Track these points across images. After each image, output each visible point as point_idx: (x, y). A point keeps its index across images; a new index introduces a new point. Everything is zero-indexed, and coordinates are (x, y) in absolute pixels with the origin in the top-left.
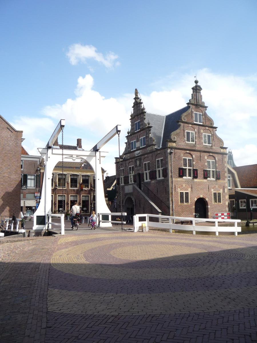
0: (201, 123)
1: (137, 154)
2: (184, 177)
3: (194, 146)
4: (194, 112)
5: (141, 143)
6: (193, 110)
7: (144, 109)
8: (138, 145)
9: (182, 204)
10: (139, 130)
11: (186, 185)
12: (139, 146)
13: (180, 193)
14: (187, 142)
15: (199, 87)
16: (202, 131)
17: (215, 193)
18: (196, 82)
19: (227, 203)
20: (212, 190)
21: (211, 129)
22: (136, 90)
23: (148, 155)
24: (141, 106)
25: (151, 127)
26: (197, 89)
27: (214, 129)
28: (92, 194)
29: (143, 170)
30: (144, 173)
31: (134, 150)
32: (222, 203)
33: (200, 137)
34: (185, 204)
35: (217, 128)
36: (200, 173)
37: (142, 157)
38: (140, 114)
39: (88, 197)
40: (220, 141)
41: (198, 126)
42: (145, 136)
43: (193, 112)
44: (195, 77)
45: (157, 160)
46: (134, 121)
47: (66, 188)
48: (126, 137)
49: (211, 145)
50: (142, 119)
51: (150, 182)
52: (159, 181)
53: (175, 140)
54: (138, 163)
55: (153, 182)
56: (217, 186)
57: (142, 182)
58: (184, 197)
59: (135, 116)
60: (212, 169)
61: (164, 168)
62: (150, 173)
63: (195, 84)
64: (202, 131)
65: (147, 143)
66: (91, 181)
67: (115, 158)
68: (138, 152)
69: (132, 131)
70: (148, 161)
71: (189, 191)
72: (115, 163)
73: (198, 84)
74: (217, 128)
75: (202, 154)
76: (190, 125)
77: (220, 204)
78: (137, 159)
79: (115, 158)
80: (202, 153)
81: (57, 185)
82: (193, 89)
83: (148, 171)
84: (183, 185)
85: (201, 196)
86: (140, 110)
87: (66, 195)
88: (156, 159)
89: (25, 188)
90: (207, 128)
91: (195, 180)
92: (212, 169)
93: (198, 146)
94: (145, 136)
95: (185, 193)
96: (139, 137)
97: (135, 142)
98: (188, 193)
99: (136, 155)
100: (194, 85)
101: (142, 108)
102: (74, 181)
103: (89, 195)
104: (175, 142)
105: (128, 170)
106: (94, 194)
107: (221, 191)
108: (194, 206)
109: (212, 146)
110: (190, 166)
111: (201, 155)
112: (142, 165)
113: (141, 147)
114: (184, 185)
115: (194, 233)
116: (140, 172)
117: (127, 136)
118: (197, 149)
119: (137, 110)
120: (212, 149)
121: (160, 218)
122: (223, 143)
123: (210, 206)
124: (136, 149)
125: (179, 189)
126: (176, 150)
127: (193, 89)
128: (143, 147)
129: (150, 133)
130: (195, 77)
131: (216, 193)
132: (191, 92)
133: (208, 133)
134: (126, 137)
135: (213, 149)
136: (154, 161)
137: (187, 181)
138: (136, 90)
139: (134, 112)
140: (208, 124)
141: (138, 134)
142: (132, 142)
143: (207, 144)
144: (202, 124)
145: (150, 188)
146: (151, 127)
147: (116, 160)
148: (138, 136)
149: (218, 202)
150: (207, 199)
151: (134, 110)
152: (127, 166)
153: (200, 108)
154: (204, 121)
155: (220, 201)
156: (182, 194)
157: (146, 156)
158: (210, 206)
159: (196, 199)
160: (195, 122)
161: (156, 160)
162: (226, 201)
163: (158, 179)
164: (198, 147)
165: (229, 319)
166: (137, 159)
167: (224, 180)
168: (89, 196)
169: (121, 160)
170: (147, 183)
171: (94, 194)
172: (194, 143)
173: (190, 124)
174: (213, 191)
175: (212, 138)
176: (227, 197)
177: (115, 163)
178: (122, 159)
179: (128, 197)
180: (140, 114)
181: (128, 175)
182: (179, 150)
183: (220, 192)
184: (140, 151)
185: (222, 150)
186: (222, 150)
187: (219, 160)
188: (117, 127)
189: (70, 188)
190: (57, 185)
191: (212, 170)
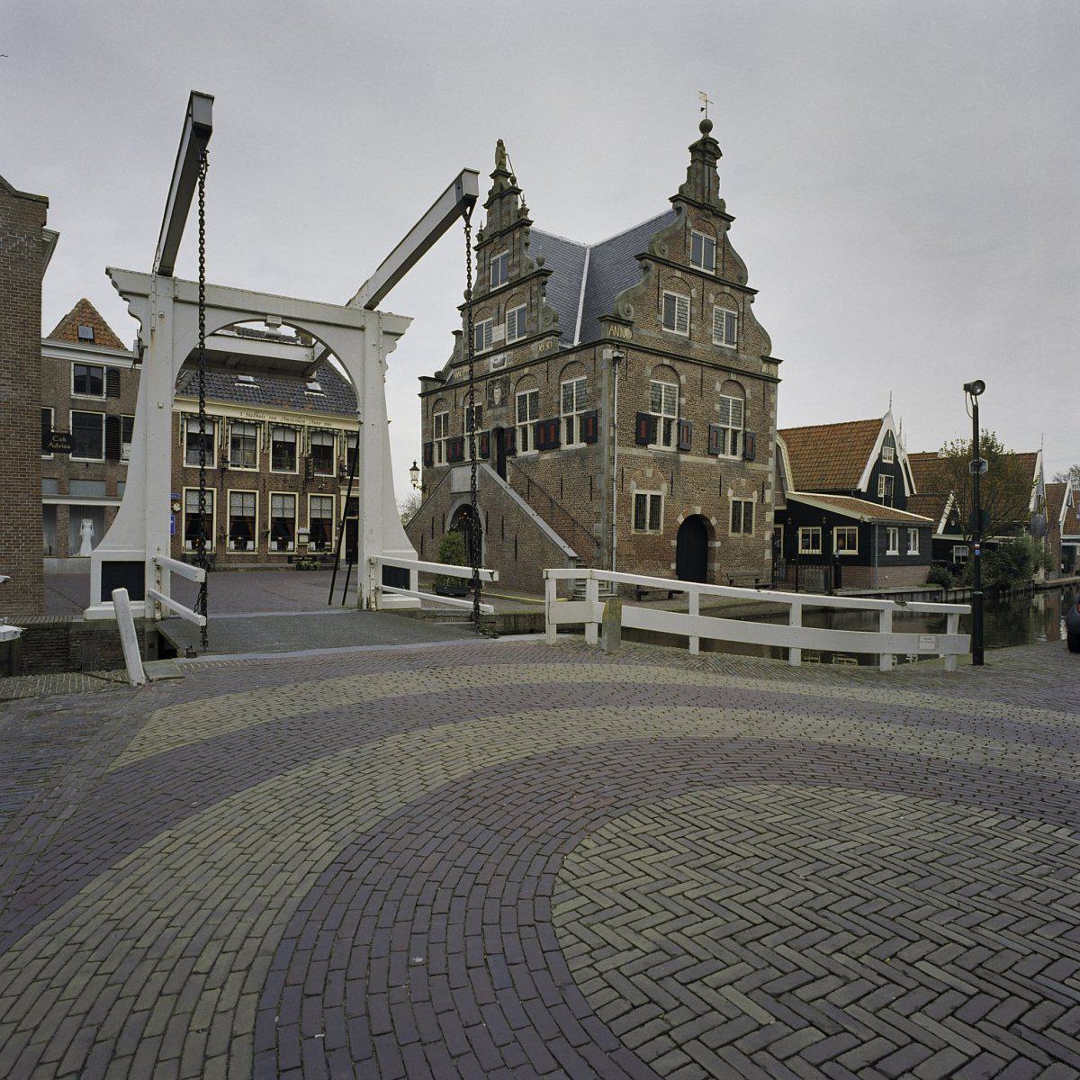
0: (712, 269)
1: (495, 366)
2: (650, 446)
3: (687, 344)
4: (693, 231)
5: (511, 328)
6: (689, 224)
7: (524, 211)
8: (499, 333)
9: (640, 532)
10: (503, 285)
11: (654, 472)
12: (503, 338)
13: (637, 495)
14: (664, 329)
15: (714, 143)
16: (712, 298)
17: (737, 502)
18: (706, 127)
19: (768, 536)
20: (730, 493)
21: (738, 295)
22: (500, 144)
23: (535, 368)
24: (517, 203)
25: (547, 273)
26: (705, 152)
27: (748, 297)
28: (344, 493)
29: (515, 417)
30: (517, 428)
31: (485, 351)
32: (753, 535)
33: (703, 318)
34: (649, 532)
35: (756, 292)
36: (699, 434)
37: (514, 376)
38: (511, 229)
39: (329, 501)
40: (763, 337)
41: (700, 280)
42: (525, 305)
43: (689, 230)
44: (702, 109)
45: (563, 383)
46: (488, 255)
47: (257, 470)
48: (459, 308)
49: (735, 347)
50: (517, 246)
51: (538, 457)
52: (569, 456)
53: (631, 318)
54: (497, 393)
55: (547, 456)
56: (743, 482)
57: (509, 458)
58: (646, 510)
59: (493, 236)
60: (733, 424)
61: (590, 410)
62: (537, 427)
63: (701, 135)
64: (712, 298)
65: (533, 327)
66: (339, 454)
67: (420, 378)
68: (500, 357)
69: (481, 289)
70: (533, 388)
71: (663, 492)
72: (420, 395)
73: (711, 135)
74: (756, 292)
75: (709, 374)
76: (678, 274)
77: (750, 536)
78: (492, 382)
79: (420, 378)
80: (708, 370)
81: (229, 460)
82: (693, 149)
83: (532, 422)
84: (648, 470)
85: (698, 511)
86: (512, 214)
87: (257, 492)
88: (560, 381)
89: (65, 447)
90: (727, 290)
91: (684, 458)
92: (733, 424)
93: (696, 345)
94: (525, 305)
95: (652, 496)
96: (433, 413)
97: (488, 324)
98: (659, 497)
99: (493, 370)
100: (699, 136)
101: (520, 207)
102: (283, 453)
103: (334, 496)
104: (629, 324)
105: (268, 610)
106: (349, 493)
107: (754, 499)
108: (675, 542)
109: (737, 351)
110: (668, 411)
111: (705, 378)
112: (510, 400)
113: (508, 343)
114: (649, 473)
115: (795, 658)
116: (505, 425)
117: (464, 305)
118: (692, 355)
119: (501, 216)
120: (736, 359)
121: (700, 605)
122: (769, 342)
123: (720, 543)
124: (491, 349)
125: (633, 483)
126: (630, 351)
127: (693, 149)
128: (517, 340)
129: (544, 295)
130: (702, 109)
131: (740, 502)
132: (687, 159)
133: (728, 306)
134: (459, 308)
135: (740, 361)
136: (554, 388)
137: (661, 461)
138: (500, 144)
139: (489, 224)
140: (730, 276)
141: (500, 296)
142: (481, 326)
143: (723, 344)
144: (713, 273)
145: (536, 478)
146: (547, 273)
147: (425, 386)
148: (503, 305)
149: (744, 531)
150: (713, 521)
151: (489, 214)
152: (461, 404)
153: (713, 220)
154: (720, 266)
155: (748, 529)
156: (641, 498)
157: (526, 370)
158: (720, 543)
159: (681, 520)
160: (692, 266)
161: (560, 386)
162: (765, 531)
163: (565, 447)
164: (697, 350)
165: (912, 1016)
166: (493, 382)
167: (766, 462)
168: (332, 497)
169: (439, 385)
170: (526, 459)
171: (349, 493)
172: (687, 335)
173: (679, 269)
174: (731, 496)
175: (741, 325)
176: (770, 517)
177: (420, 395)
178: (443, 382)
179: (462, 505)
180: (511, 229)
181: (460, 435)
182: (640, 355)
183: (750, 500)
184: (506, 354)
185: (765, 368)
186: (765, 368)
187: (755, 397)
188: (458, 182)
189: (271, 471)
190: (229, 460)
191: (732, 430)
